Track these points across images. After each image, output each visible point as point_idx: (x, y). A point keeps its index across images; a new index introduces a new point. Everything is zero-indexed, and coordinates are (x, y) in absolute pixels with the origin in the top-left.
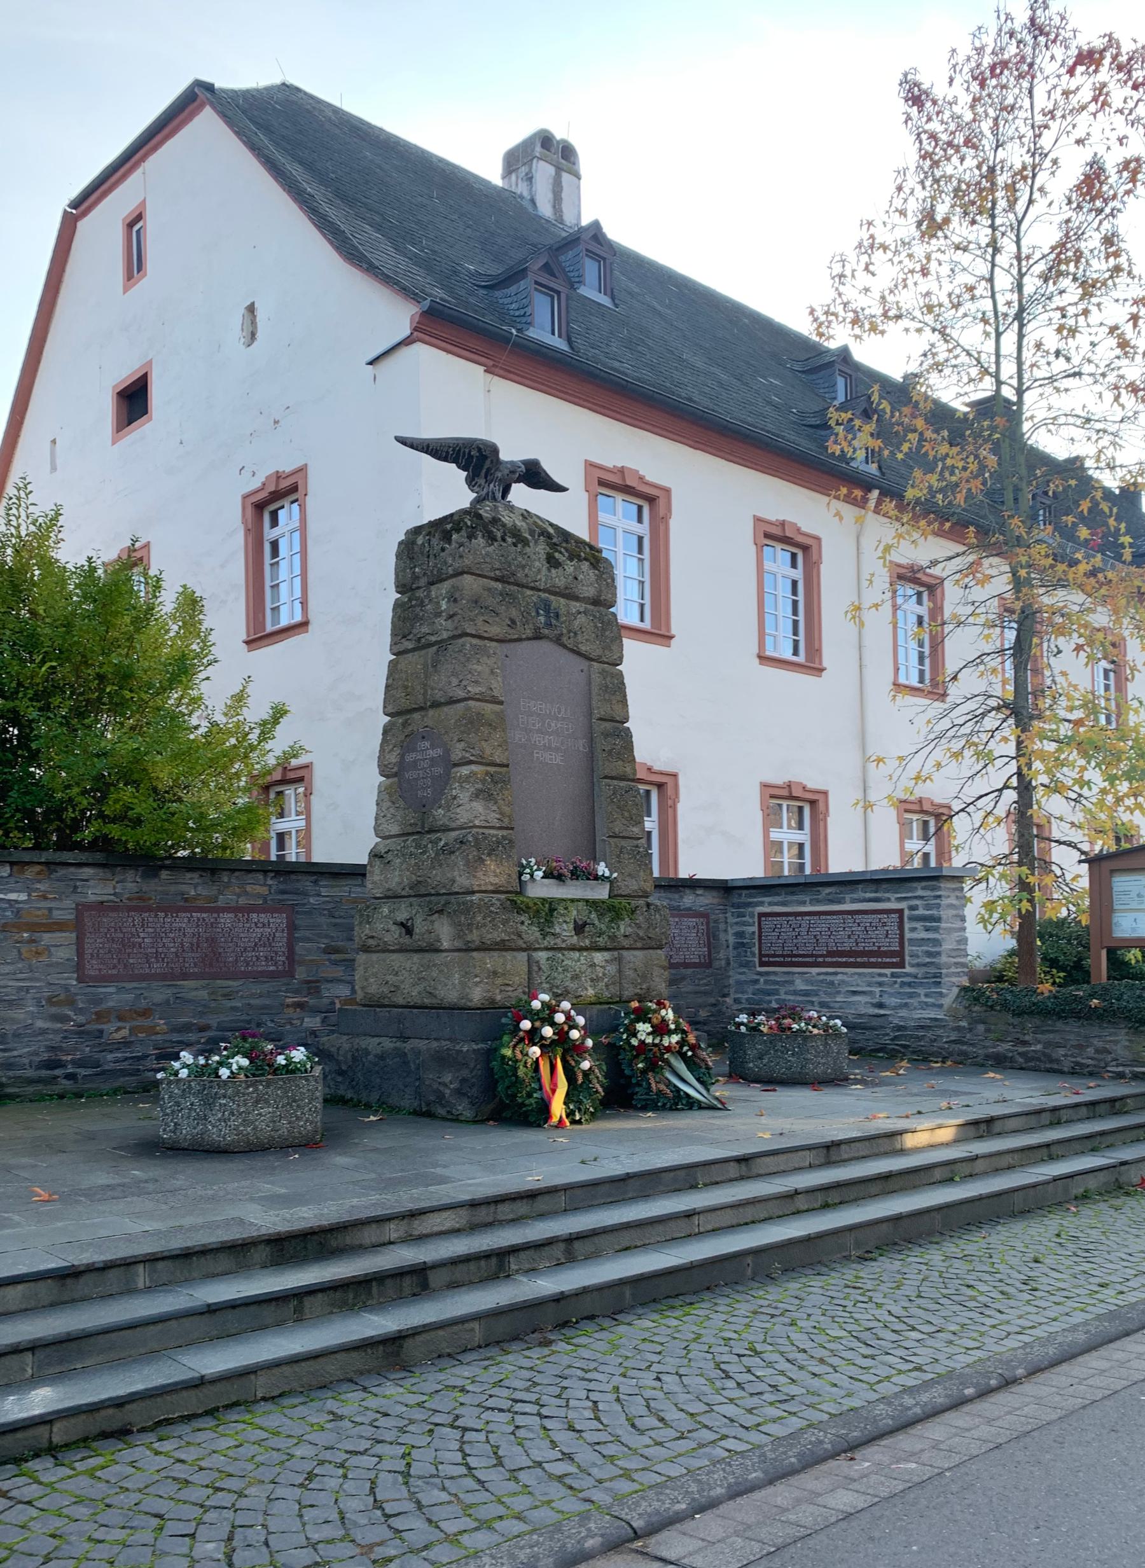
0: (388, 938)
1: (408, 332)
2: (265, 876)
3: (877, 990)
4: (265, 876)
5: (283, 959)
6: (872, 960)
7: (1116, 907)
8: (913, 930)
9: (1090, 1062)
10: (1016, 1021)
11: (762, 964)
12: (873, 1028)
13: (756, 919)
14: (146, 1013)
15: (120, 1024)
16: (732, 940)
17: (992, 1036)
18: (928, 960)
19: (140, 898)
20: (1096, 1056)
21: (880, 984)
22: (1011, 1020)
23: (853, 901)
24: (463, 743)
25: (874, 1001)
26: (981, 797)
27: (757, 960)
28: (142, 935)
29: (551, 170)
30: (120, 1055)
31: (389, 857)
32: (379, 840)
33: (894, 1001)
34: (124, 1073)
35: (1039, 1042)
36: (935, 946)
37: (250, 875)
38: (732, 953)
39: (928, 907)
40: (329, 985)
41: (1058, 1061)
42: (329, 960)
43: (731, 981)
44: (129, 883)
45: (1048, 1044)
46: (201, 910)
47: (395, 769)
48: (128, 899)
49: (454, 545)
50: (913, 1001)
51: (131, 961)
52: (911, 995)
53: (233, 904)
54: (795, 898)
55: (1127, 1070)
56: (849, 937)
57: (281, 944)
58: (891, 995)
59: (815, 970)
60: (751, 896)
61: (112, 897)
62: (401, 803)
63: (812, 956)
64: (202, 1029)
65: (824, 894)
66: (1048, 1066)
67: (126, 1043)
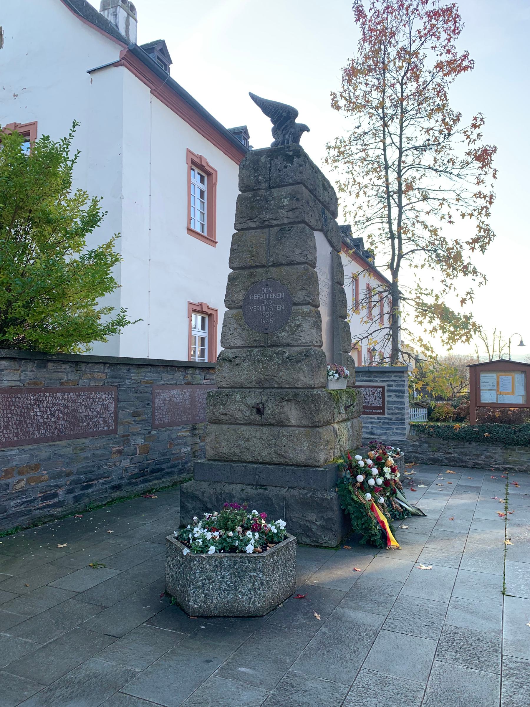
0: (239, 415)
1: (118, 59)
2: (104, 367)
3: (370, 426)
4: (104, 367)
5: (111, 422)
7: (481, 388)
8: (390, 396)
9: (482, 462)
10: (445, 442)
14: (36, 467)
15: (20, 477)
17: (431, 449)
18: (398, 411)
19: (35, 383)
20: (486, 459)
21: (371, 423)
22: (442, 442)
24: (304, 291)
25: (368, 431)
26: (375, 331)
28: (35, 410)
29: (126, 14)
30: (19, 501)
31: (237, 361)
32: (224, 349)
33: (379, 431)
34: (22, 514)
35: (457, 453)
36: (400, 405)
37: (97, 366)
39: (397, 386)
40: (134, 437)
41: (466, 462)
42: (134, 421)
44: (28, 373)
45: (461, 454)
46: (70, 390)
47: (241, 304)
48: (28, 384)
49: (295, 165)
51: (28, 429)
52: (388, 429)
53: (87, 386)
55: (501, 466)
57: (111, 412)
58: (377, 428)
61: (18, 383)
62: (246, 326)
64: (68, 475)
66: (461, 464)
67: (23, 492)
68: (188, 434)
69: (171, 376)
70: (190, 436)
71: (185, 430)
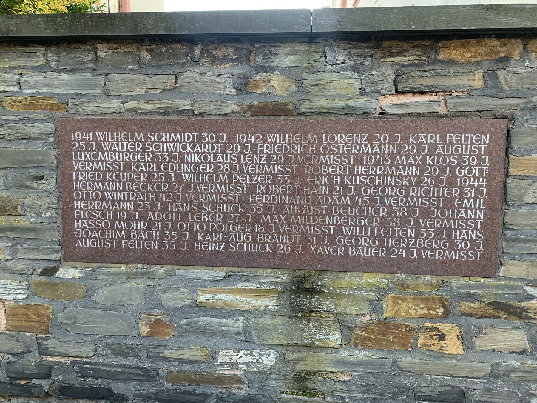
68: (270, 303)
69: (164, 80)
70: (275, 314)
71: (241, 285)
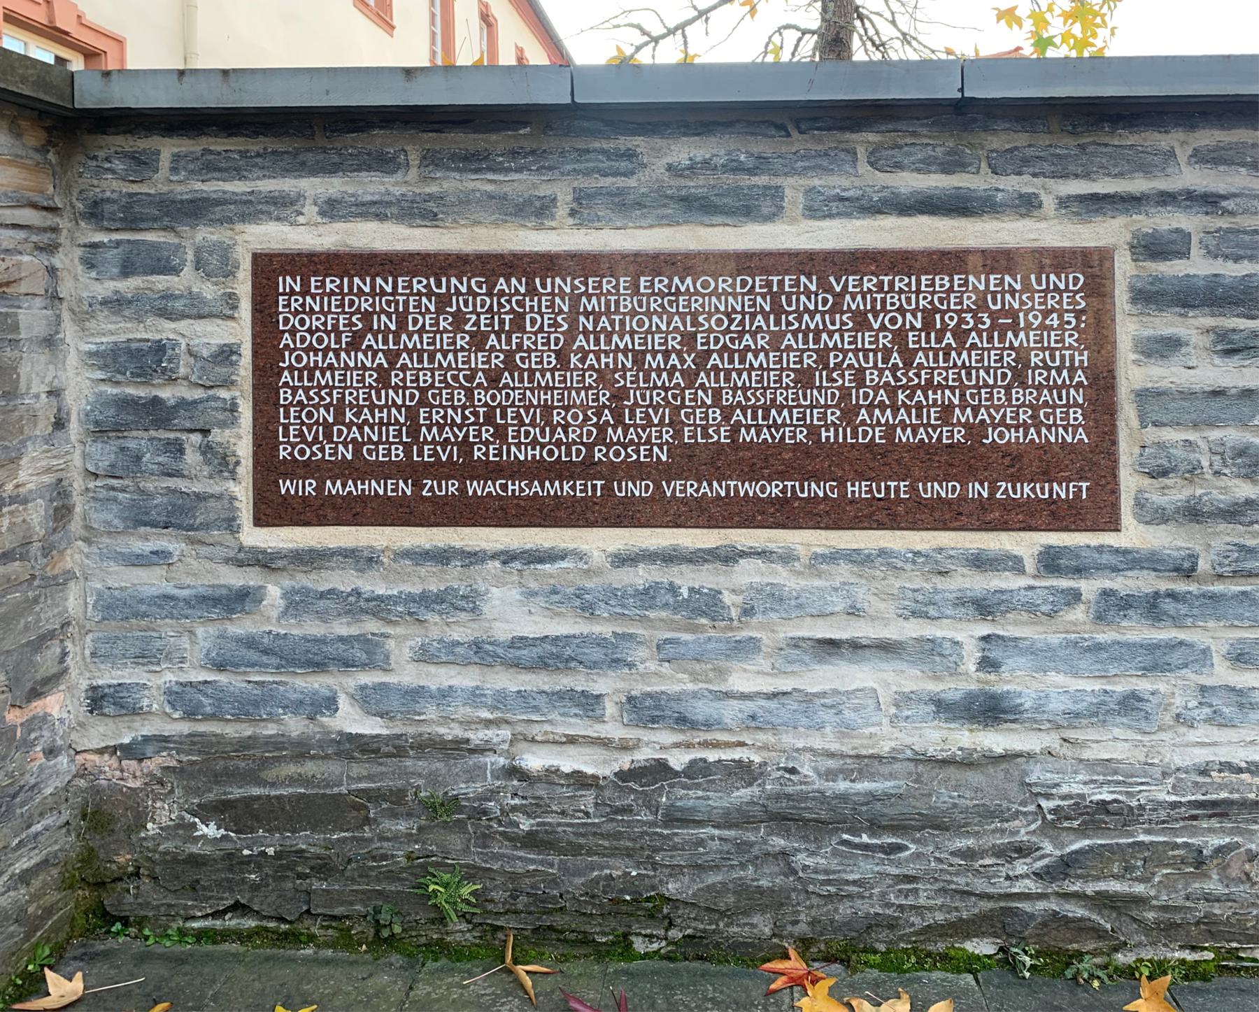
3: (967, 634)
6: (858, 489)
8: (1165, 347)
11: (271, 510)
12: (938, 824)
13: (243, 287)
16: (82, 387)
21: (984, 608)
23: (818, 209)
25: (953, 689)
27: (242, 491)
33: (1062, 687)
38: (78, 454)
43: (73, 601)
50: (1174, 690)
52: (1157, 660)
54: (480, 184)
56: (804, 379)
58: (1044, 657)
59: (599, 542)
60: (210, 168)
63: (588, 468)
65: (658, 167)
